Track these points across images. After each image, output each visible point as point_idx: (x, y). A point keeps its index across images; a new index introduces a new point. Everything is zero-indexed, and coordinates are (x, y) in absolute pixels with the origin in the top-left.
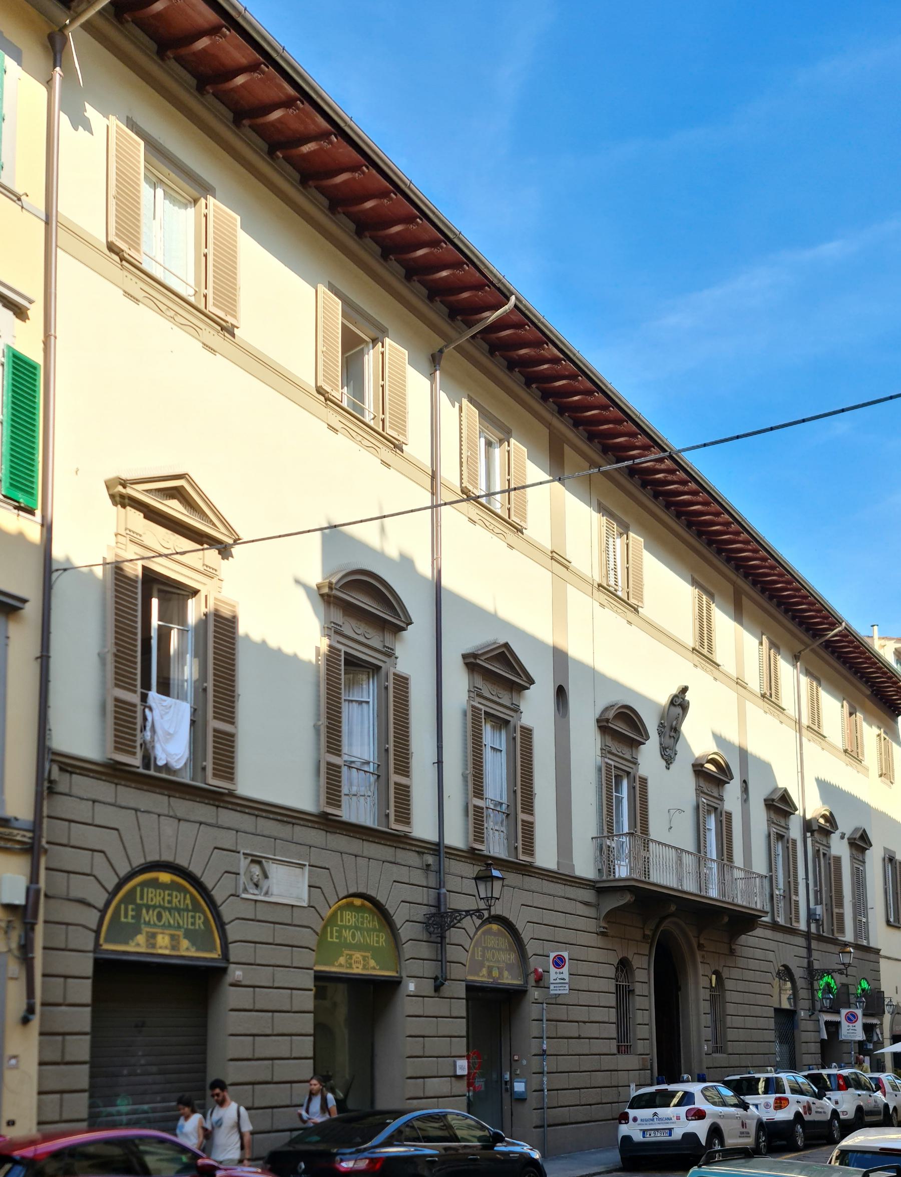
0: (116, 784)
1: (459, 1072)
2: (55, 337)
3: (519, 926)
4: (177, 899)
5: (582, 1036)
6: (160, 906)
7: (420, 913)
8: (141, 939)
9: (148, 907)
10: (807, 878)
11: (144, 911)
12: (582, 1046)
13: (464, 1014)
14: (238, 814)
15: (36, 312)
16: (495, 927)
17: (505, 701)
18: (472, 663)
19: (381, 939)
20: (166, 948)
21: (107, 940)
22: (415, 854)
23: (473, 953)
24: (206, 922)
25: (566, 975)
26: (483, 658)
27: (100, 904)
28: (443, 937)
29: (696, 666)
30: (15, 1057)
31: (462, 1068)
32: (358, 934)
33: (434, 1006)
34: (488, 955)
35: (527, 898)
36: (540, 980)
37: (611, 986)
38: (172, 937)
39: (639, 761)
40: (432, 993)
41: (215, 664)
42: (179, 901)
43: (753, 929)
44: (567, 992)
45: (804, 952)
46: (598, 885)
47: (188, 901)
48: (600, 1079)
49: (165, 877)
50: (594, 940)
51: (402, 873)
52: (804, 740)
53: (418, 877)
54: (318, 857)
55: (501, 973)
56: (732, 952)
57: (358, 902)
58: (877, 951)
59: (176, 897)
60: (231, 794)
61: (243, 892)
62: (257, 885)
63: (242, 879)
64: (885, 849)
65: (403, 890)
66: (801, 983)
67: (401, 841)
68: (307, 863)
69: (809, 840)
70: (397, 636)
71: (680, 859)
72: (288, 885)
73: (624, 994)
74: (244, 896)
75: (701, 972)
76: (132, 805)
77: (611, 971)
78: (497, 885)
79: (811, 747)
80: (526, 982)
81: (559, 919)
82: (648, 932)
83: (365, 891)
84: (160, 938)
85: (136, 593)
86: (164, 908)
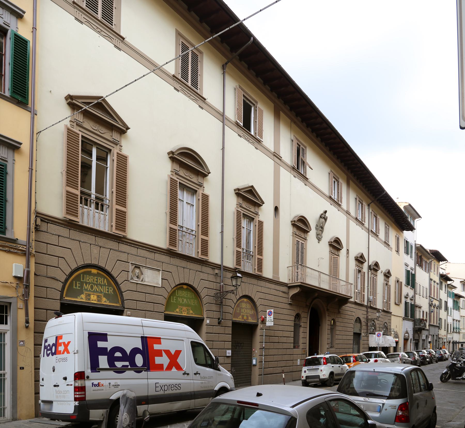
0: (119, 243)
1: (228, 355)
3: (255, 300)
4: (100, 280)
6: (92, 283)
7: (213, 293)
8: (83, 296)
9: (86, 283)
10: (368, 286)
11: (84, 284)
12: (280, 346)
13: (231, 333)
14: (129, 247)
15: (28, 16)
16: (245, 300)
17: (252, 210)
18: (239, 193)
19: (194, 302)
20: (95, 300)
21: (66, 296)
22: (211, 269)
23: (236, 310)
24: (114, 290)
25: (272, 319)
26: (242, 191)
27: (63, 280)
28: (222, 302)
29: (331, 204)
30: (22, 341)
31: (229, 353)
32: (185, 300)
33: (218, 329)
34: (243, 310)
35: (259, 289)
36: (264, 321)
37: (292, 323)
38: (98, 296)
39: (307, 239)
40: (217, 324)
41: (117, 179)
42: (101, 282)
43: (346, 303)
45: (365, 313)
46: (289, 285)
47: (105, 281)
48: (286, 357)
49: (94, 271)
50: (288, 307)
51: (205, 276)
52: (370, 236)
53: (212, 278)
54: (165, 267)
55: (247, 316)
56: (339, 312)
57: (185, 287)
58: (391, 313)
59: (100, 280)
60: (125, 237)
61: (131, 279)
62: (138, 277)
63: (130, 274)
64: (396, 277)
65: (202, 280)
66: (363, 324)
67: (204, 263)
69: (370, 273)
70: (205, 178)
71: (320, 275)
72: (152, 278)
73: (297, 327)
75: (327, 319)
76: (78, 239)
77: (293, 318)
78: (239, 280)
79: (372, 239)
80: (258, 321)
81: (273, 298)
82: (308, 304)
83: (187, 282)
84: (92, 296)
85: (79, 145)
86: (94, 284)
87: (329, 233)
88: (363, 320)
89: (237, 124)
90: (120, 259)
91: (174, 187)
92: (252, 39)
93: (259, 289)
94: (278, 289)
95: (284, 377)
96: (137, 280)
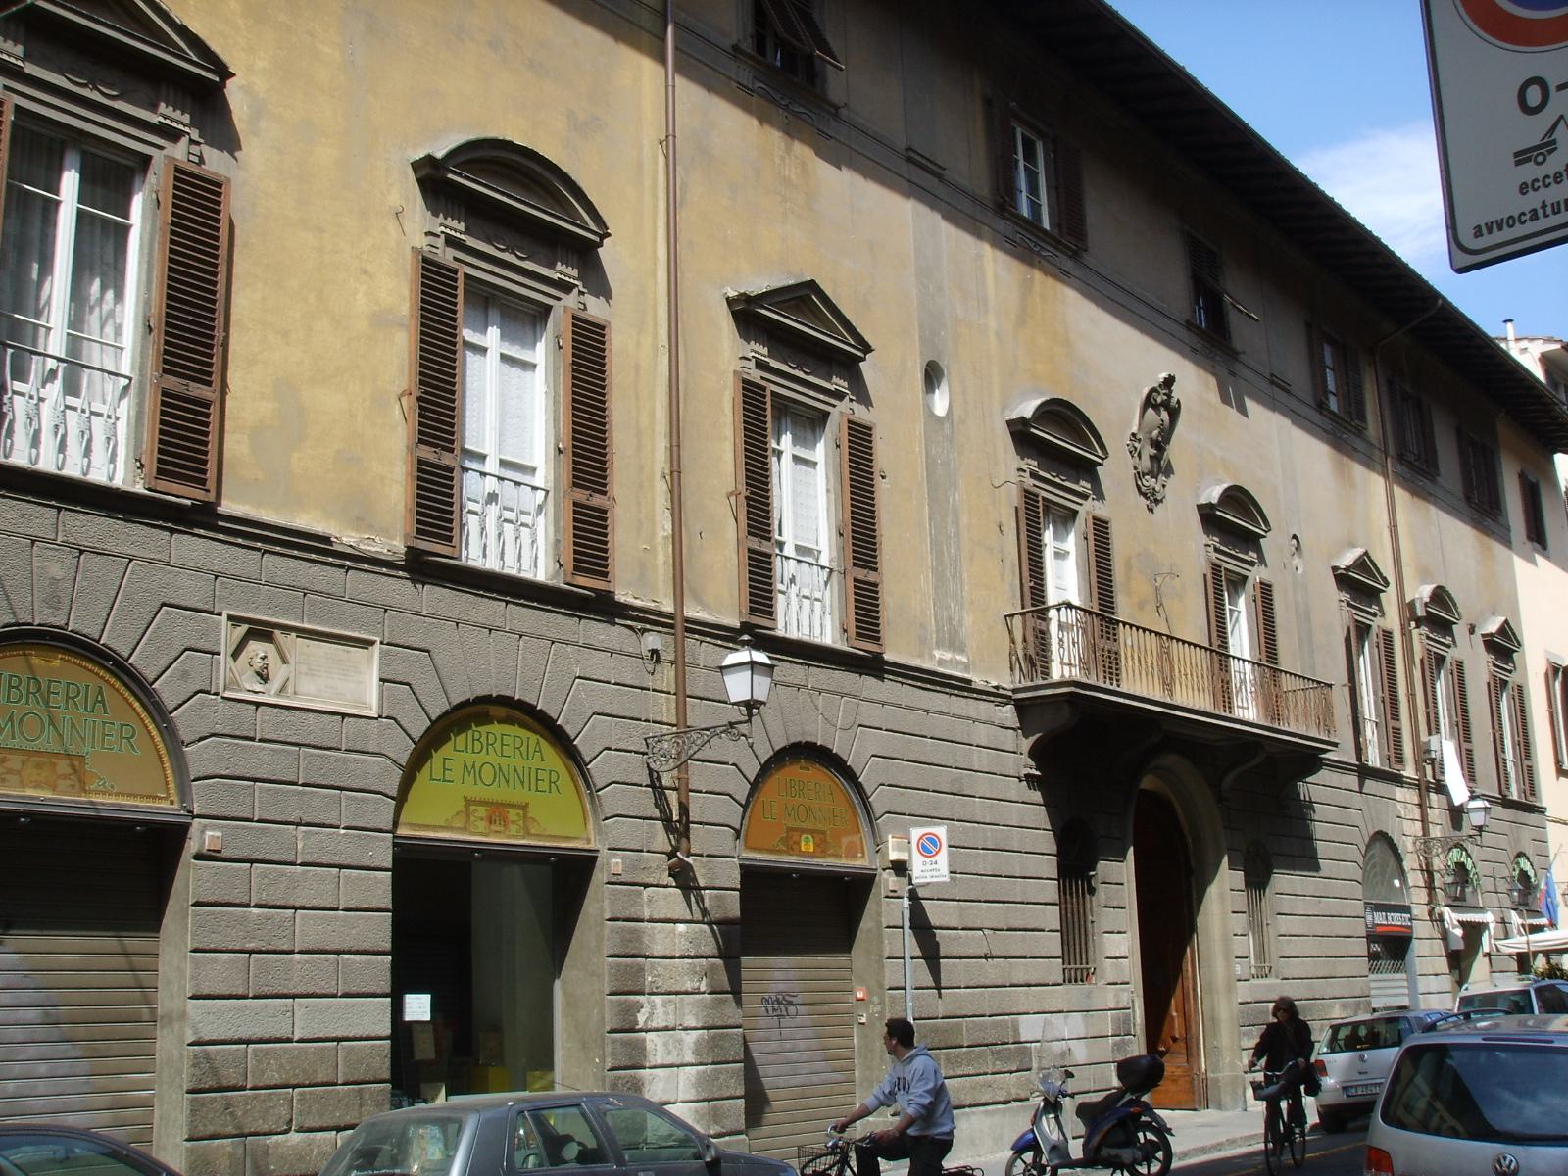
2: (675, 137)
5: (994, 953)
43: (1313, 770)
44: (947, 879)
58: (1542, 811)
68: (378, 639)
72: (345, 683)
74: (227, 694)
87: (1202, 472)
88: (1407, 845)
89: (1189, 325)
90: (172, 601)
91: (762, 416)
92: (1440, 301)
93: (871, 714)
94: (963, 713)
95: (1143, 1119)
96: (258, 687)
